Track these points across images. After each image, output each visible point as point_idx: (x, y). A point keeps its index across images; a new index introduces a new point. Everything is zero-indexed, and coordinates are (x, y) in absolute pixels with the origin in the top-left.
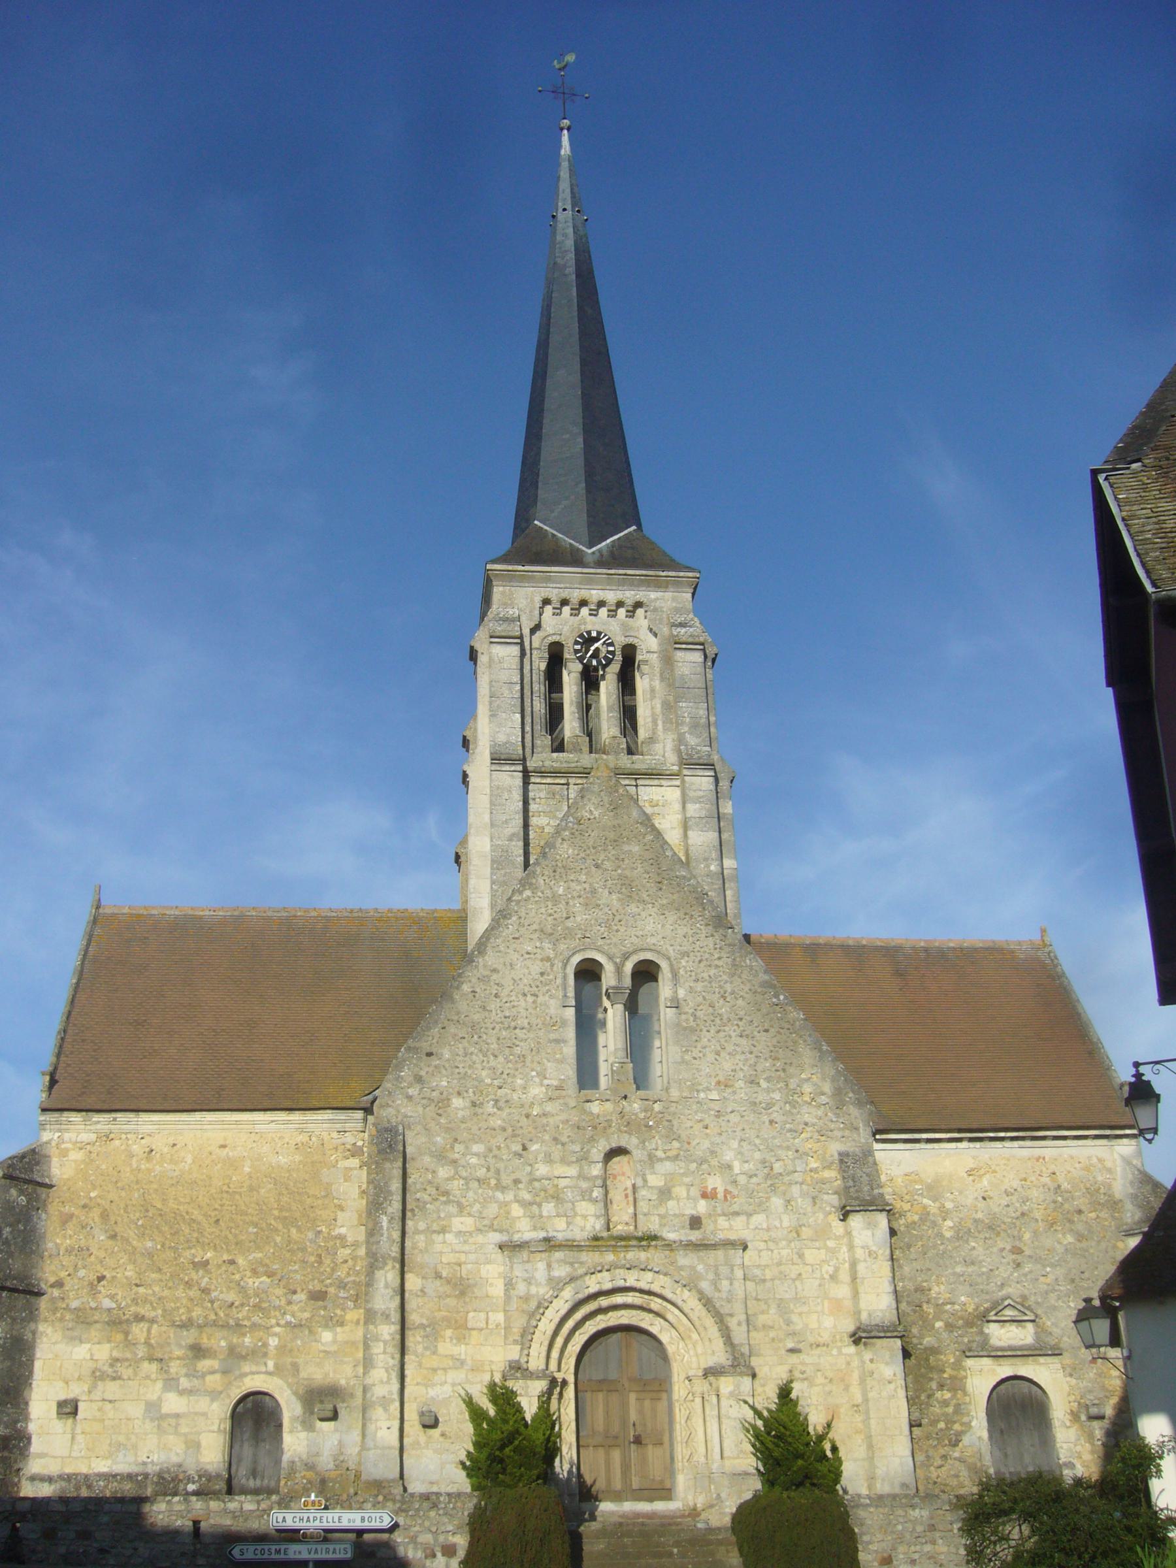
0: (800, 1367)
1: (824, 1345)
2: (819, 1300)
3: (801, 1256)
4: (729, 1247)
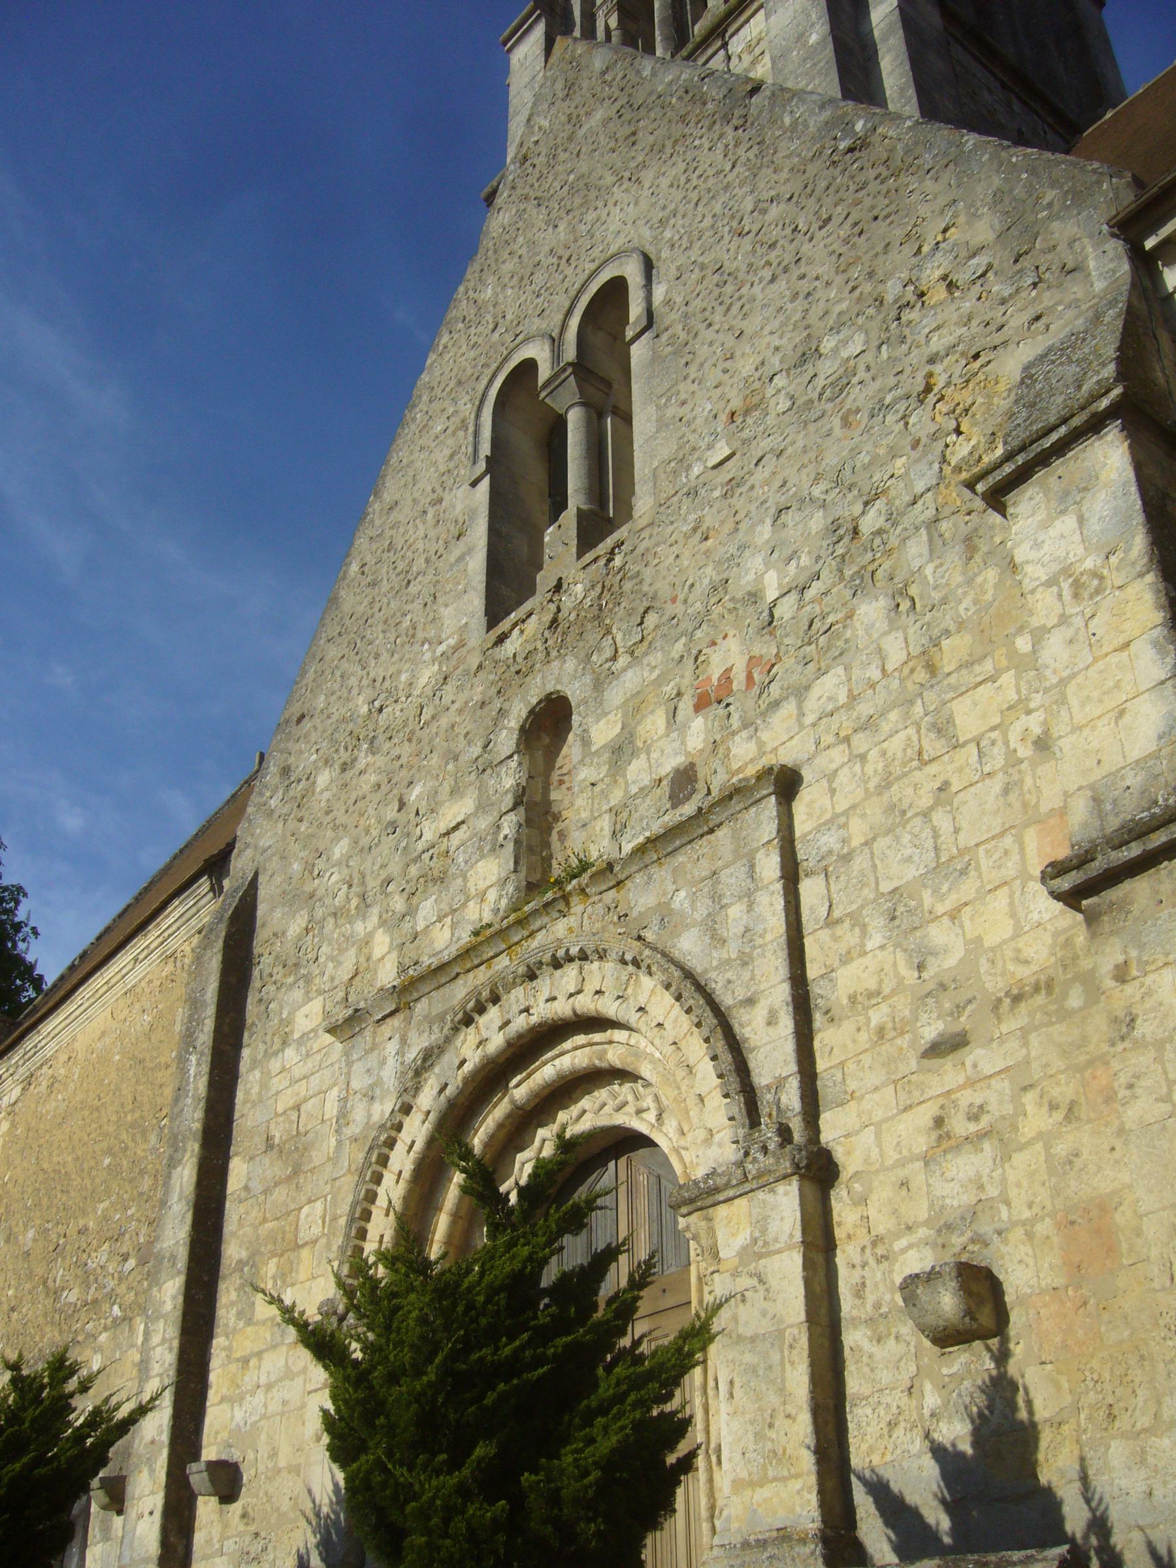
0: (967, 1098)
1: (1037, 989)
2: (1008, 841)
3: (943, 728)
4: (736, 805)
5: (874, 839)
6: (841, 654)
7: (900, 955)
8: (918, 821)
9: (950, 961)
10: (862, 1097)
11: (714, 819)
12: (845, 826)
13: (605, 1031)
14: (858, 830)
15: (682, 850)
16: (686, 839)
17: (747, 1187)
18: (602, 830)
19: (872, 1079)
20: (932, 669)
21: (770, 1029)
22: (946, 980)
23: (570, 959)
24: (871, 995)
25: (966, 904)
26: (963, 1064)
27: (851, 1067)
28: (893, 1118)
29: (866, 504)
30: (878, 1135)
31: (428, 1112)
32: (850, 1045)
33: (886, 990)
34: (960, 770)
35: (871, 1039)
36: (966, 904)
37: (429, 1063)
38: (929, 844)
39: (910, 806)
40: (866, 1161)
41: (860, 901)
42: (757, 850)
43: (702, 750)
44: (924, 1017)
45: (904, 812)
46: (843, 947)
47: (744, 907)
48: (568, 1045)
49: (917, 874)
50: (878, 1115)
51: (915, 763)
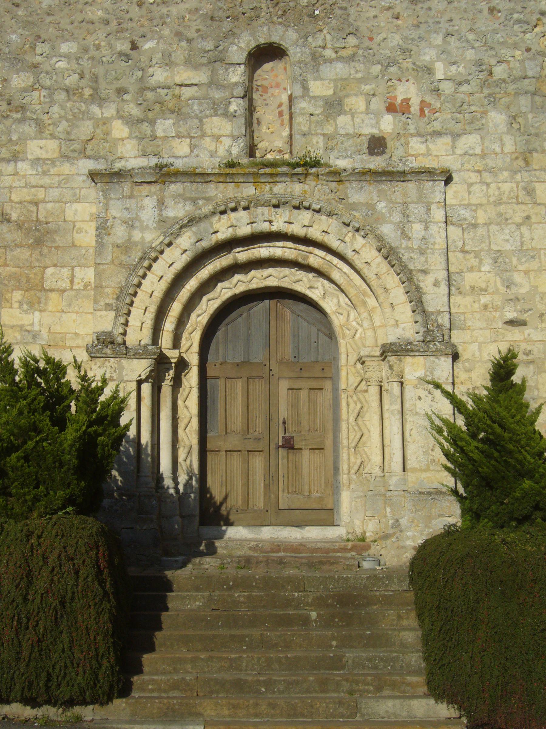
5: (490, 224)
6: (479, 129)
7: (498, 279)
8: (513, 227)
9: (523, 291)
10: (474, 330)
11: (409, 177)
12: (475, 211)
13: (309, 246)
14: (482, 217)
15: (385, 183)
16: (390, 179)
17: (427, 353)
18: (317, 143)
19: (479, 324)
20: (527, 163)
21: (435, 288)
22: (520, 297)
23: (308, 208)
24: (482, 290)
25: (532, 271)
26: (523, 332)
27: (469, 316)
28: (488, 343)
29: (498, 62)
30: (480, 348)
31: (185, 251)
32: (469, 307)
33: (490, 291)
34: (536, 214)
35: (480, 308)
36: (532, 271)
37: (190, 224)
38: (518, 238)
39: (510, 218)
40: (473, 355)
41: (480, 248)
42: (433, 203)
43: (391, 134)
44: (507, 308)
45: (507, 220)
46: (469, 265)
47: (423, 227)
48: (281, 244)
49: (511, 249)
50: (481, 339)
51: (514, 201)
